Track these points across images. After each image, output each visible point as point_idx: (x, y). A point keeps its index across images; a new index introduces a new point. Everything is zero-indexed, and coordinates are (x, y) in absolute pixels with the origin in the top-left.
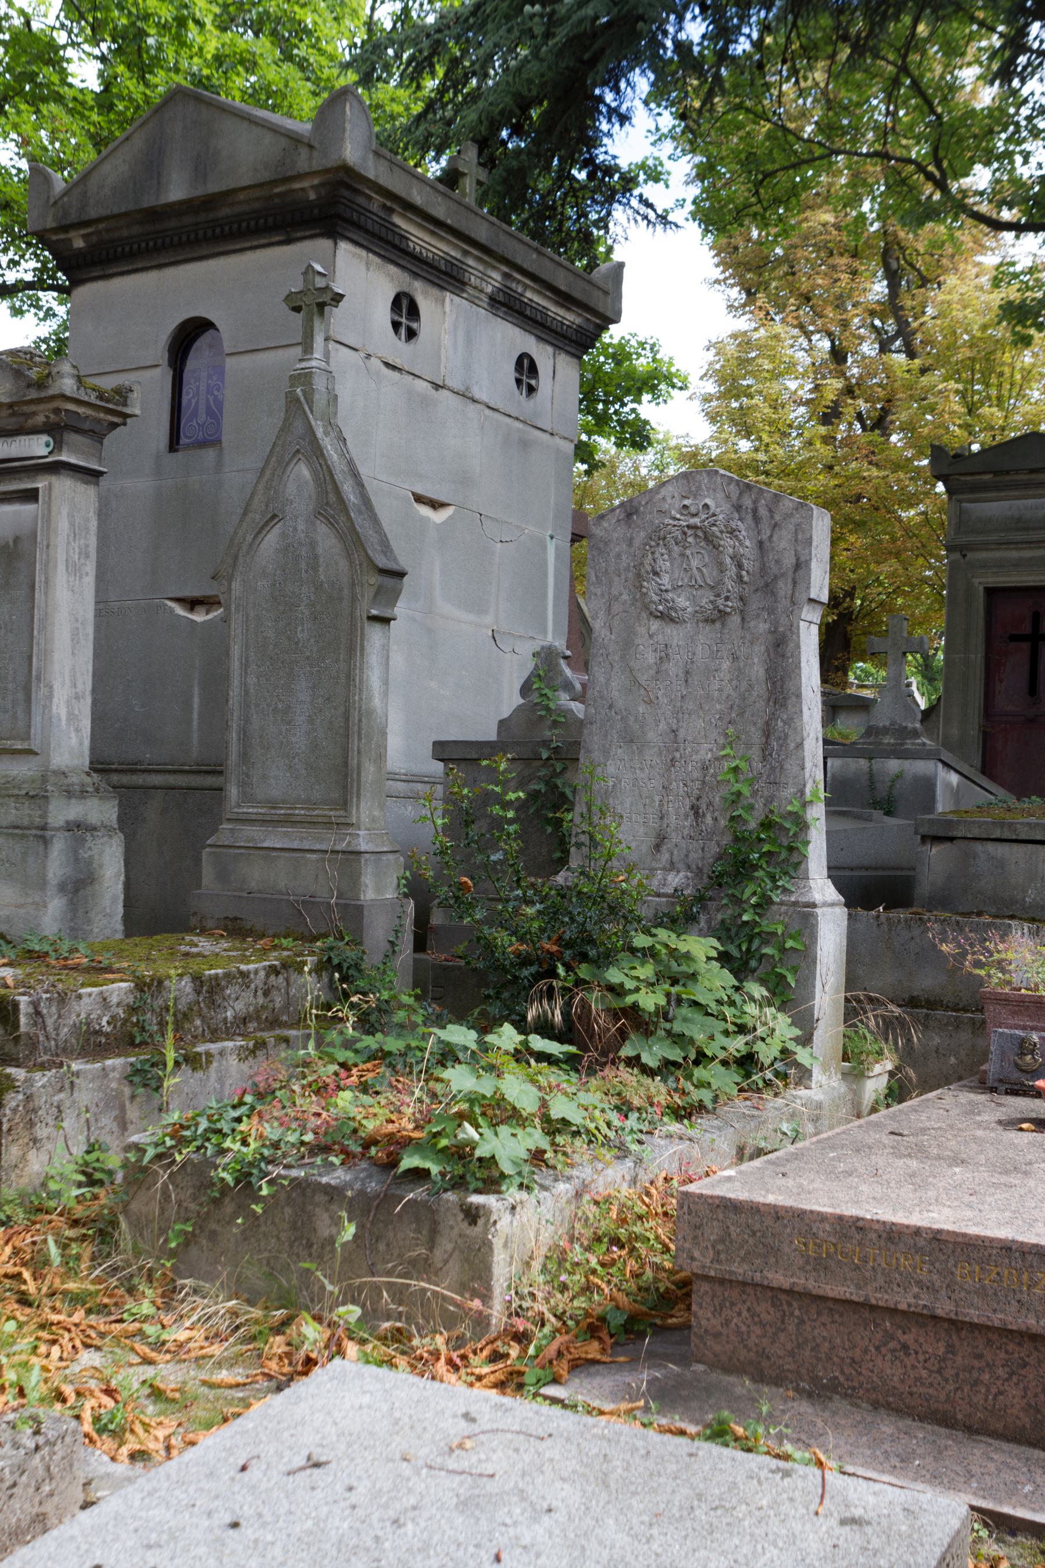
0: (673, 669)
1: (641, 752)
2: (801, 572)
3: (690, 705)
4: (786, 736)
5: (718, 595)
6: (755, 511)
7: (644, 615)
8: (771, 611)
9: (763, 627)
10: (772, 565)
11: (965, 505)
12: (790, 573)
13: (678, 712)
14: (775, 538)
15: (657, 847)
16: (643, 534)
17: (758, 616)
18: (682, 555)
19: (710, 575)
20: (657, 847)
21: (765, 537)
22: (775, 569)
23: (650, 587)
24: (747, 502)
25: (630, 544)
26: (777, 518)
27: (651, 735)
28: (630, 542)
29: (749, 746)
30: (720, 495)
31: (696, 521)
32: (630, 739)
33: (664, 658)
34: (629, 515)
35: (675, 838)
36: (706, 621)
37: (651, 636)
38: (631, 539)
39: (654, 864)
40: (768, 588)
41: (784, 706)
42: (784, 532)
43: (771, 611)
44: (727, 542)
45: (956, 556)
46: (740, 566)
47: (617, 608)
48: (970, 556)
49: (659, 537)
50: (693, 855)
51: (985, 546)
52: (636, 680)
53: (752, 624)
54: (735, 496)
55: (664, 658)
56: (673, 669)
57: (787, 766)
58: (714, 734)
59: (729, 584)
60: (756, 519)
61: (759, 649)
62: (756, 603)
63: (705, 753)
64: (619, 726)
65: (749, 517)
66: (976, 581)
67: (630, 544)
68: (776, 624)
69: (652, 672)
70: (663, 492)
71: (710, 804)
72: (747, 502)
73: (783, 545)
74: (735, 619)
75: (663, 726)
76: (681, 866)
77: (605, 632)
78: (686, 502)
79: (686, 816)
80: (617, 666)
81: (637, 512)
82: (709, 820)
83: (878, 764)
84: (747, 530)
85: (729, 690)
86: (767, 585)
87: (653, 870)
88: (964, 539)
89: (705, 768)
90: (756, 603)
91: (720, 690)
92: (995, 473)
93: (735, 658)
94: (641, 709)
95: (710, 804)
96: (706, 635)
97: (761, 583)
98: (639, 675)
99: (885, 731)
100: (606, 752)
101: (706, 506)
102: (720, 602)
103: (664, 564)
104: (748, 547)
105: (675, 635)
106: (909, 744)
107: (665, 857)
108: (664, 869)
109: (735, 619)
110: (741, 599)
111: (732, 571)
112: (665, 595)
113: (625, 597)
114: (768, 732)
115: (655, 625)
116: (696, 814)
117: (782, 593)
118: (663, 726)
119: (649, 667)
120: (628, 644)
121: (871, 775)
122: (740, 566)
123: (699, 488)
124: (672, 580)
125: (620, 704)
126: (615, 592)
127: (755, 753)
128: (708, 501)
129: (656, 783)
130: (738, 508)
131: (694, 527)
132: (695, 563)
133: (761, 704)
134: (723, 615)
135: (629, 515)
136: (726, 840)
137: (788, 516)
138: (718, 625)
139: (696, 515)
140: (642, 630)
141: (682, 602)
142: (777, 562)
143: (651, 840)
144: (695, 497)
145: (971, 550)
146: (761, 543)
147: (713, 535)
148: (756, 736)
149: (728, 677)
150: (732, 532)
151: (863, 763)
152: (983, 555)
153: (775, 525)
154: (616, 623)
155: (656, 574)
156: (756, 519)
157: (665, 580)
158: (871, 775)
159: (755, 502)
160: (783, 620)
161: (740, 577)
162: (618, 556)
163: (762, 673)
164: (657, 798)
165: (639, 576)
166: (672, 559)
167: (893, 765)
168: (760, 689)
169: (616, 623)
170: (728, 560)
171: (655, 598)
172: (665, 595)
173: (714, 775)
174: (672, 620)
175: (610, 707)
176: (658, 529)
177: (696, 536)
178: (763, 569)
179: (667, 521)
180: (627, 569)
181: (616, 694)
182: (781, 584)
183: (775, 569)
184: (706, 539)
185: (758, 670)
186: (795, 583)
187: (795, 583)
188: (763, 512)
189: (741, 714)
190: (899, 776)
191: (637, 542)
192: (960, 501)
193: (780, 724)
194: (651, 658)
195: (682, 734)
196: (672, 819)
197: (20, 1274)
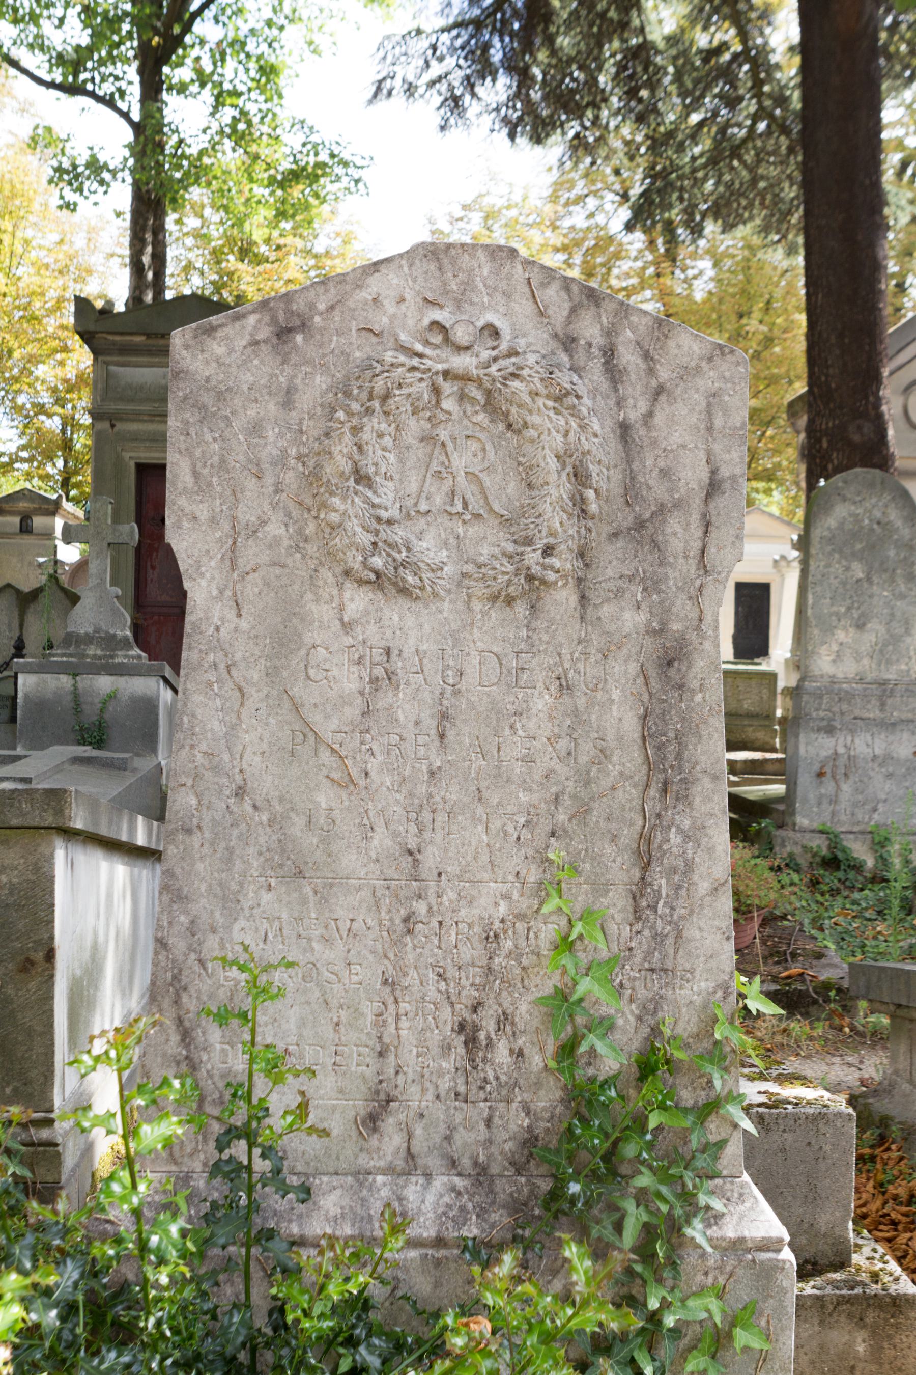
0: (409, 707)
1: (324, 901)
2: (720, 502)
3: (452, 792)
4: (689, 866)
6: (609, 353)
7: (327, 575)
8: (652, 585)
9: (631, 619)
10: (653, 479)
11: (113, 368)
12: (697, 502)
13: (421, 812)
14: (659, 419)
15: (372, 1121)
16: (321, 381)
17: (619, 593)
19: (505, 490)
20: (372, 1121)
22: (659, 491)
24: (590, 329)
26: (664, 374)
27: (350, 861)
28: (288, 399)
29: (601, 888)
31: (462, 362)
32: (290, 867)
33: (384, 678)
34: (283, 333)
35: (415, 1098)
37: (347, 627)
38: (290, 391)
39: (363, 1161)
40: (644, 531)
41: (683, 798)
42: (681, 409)
43: (652, 585)
45: (106, 425)
46: (580, 476)
47: (252, 553)
48: (120, 426)
49: (363, 392)
50: (462, 1137)
51: (136, 417)
52: (309, 731)
53: (606, 611)
55: (384, 678)
56: (409, 707)
57: (691, 932)
58: (513, 861)
60: (614, 373)
61: (623, 671)
62: (612, 562)
63: (492, 901)
64: (264, 837)
65: (596, 366)
66: (126, 455)
68: (664, 612)
69: (352, 712)
70: (375, 285)
71: (504, 1019)
72: (590, 329)
73: (676, 438)
75: (381, 840)
76: (434, 1162)
77: (221, 612)
79: (446, 1048)
80: (255, 697)
82: (502, 1054)
83: (84, 681)
84: (594, 392)
85: (546, 761)
86: (640, 525)
87: (361, 1175)
88: (112, 407)
89: (491, 938)
90: (612, 562)
91: (529, 760)
92: (148, 336)
93: (565, 687)
94: (324, 798)
95: (504, 1019)
96: (492, 632)
97: (626, 519)
98: (315, 718)
99: (88, 639)
100: (230, 902)
102: (532, 557)
103: (380, 458)
105: (410, 628)
106: (120, 658)
107: (391, 1142)
108: (389, 1170)
109: (564, 597)
110: (581, 555)
111: (559, 488)
112: (386, 533)
113: (275, 529)
114: (645, 856)
115: (357, 601)
116: (471, 1042)
117: (676, 545)
118: (381, 840)
119: (345, 701)
120: (284, 642)
121: (76, 694)
122: (580, 476)
123: (468, 286)
125: (266, 785)
126: (247, 515)
127: (616, 904)
129: (368, 973)
130: (568, 342)
131: (464, 378)
132: (460, 461)
133: (628, 794)
135: (283, 333)
136: (548, 1098)
137: (688, 373)
138: (521, 609)
140: (323, 612)
141: (429, 547)
142: (665, 473)
143: (359, 1105)
145: (121, 419)
146: (624, 429)
148: (620, 868)
149: (547, 730)
150: (561, 398)
151: (65, 681)
152: (134, 427)
153: (660, 390)
154: (251, 589)
155: (362, 478)
156: (614, 373)
157: (386, 495)
158: (76, 694)
159: (609, 333)
160: (682, 607)
161: (579, 502)
162: (256, 429)
163: (631, 726)
164: (369, 1009)
166: (401, 449)
167: (104, 683)
168: (628, 760)
169: (251, 589)
171: (365, 539)
172: (386, 533)
173: (515, 954)
174: (404, 591)
175: (240, 792)
177: (462, 397)
178: (631, 491)
180: (281, 461)
181: (253, 761)
182: (674, 524)
183: (659, 491)
184: (490, 405)
185: (621, 718)
186: (707, 526)
187: (707, 526)
188: (628, 357)
189: (581, 813)
190: (112, 697)
191: (306, 399)
192: (107, 363)
193: (675, 838)
194: (349, 680)
195: (430, 859)
196: (410, 1057)
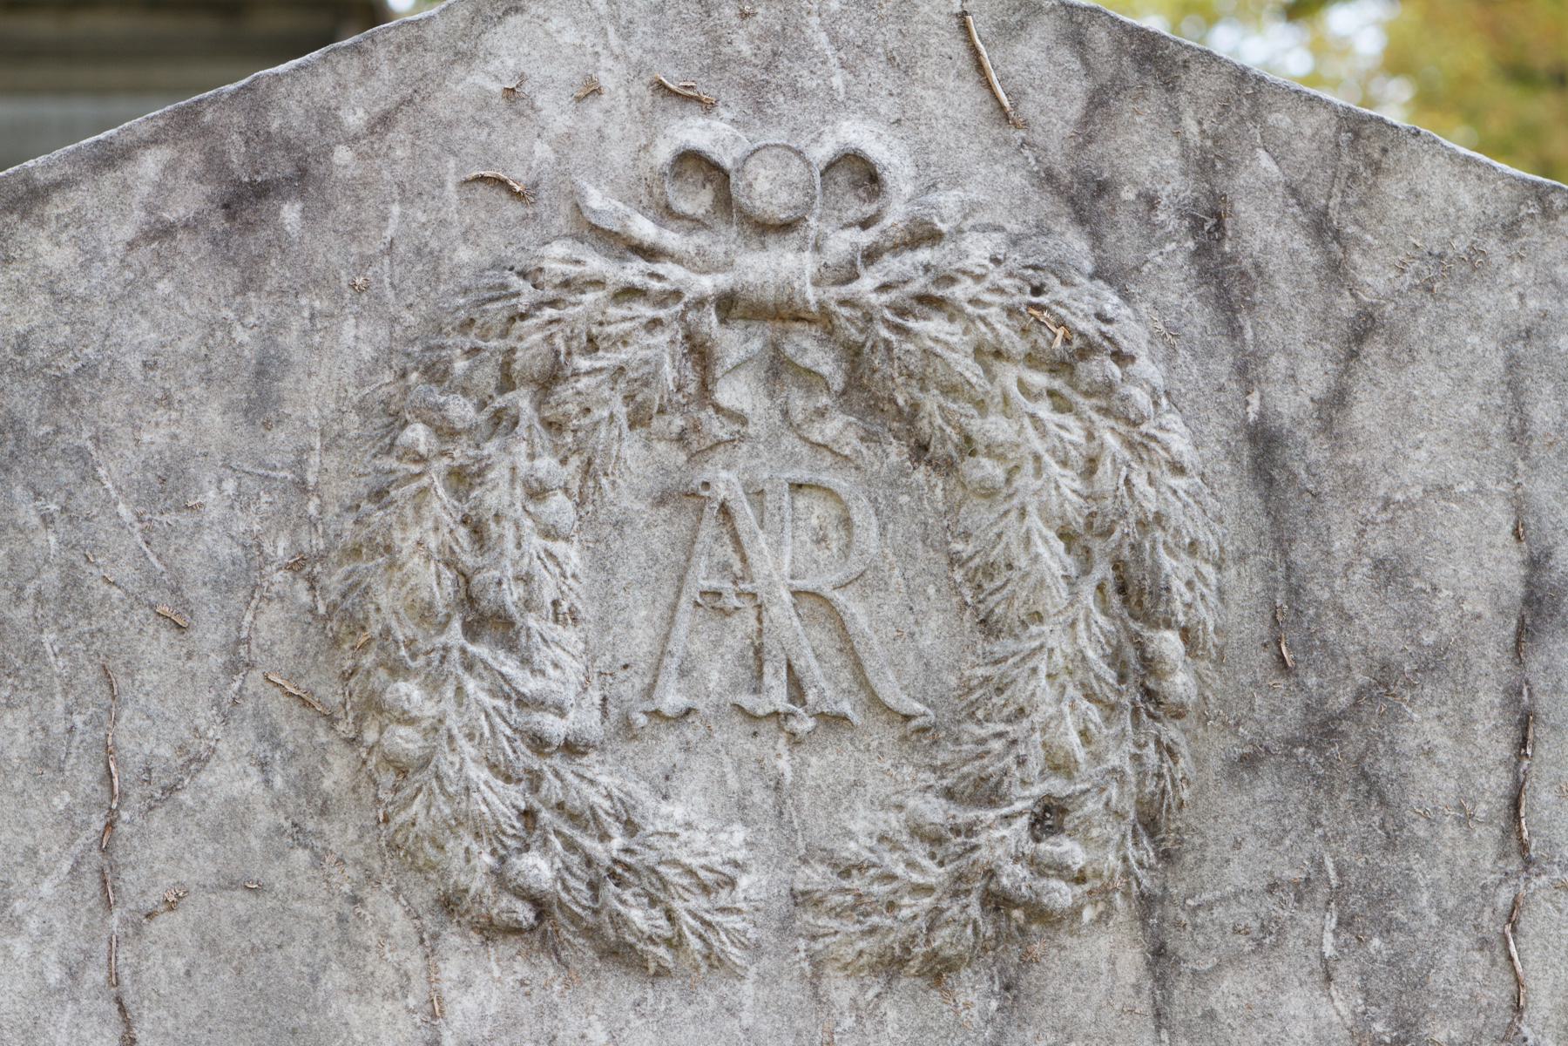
5: (988, 792)
6: (1210, 223)
7: (389, 913)
8: (1365, 908)
14: (1365, 411)
16: (357, 337)
17: (1267, 938)
18: (680, 497)
19: (911, 641)
21: (1290, 400)
22: (1374, 625)
23: (446, 713)
25: (260, 402)
26: (1375, 277)
30: (950, 100)
36: (891, 965)
42: (1429, 380)
43: (1365, 908)
44: (1038, 448)
46: (1135, 593)
47: (161, 855)
53: (1231, 991)
54: (1055, 106)
59: (1064, 718)
62: (1244, 845)
67: (260, 402)
73: (1422, 464)
74: (1099, 961)
78: (696, 132)
81: (304, 178)
84: (1168, 340)
86: (1323, 729)
90: (1244, 845)
97: (1278, 713)
101: (862, 174)
102: (1002, 839)
103: (542, 558)
104: (1186, 489)
110: (1149, 822)
111: (1073, 627)
112: (564, 781)
113: (230, 778)
117: (1433, 786)
122: (1135, 593)
124: (601, 672)
128: (856, 133)
130: (1086, 197)
132: (780, 559)
134: (1013, 921)
137: (1445, 272)
138: (974, 995)
139: (768, 229)
141: (691, 820)
142: (1389, 572)
144: (757, 98)
146: (1263, 447)
147: (927, 370)
153: (1365, 326)
154: (161, 960)
155: (487, 620)
157: (560, 669)
159: (1208, 163)
161: (1139, 673)
162: (168, 483)
165: (341, 624)
166: (601, 530)
169: (161, 960)
170: (1053, 558)
172: (564, 781)
174: (621, 953)
176: (495, 301)
177: (778, 369)
178: (1289, 627)
179: (557, 257)
180: (243, 577)
182: (1423, 722)
183: (1374, 625)
184: (862, 389)
188: (1267, 233)
197: (504, 286)
